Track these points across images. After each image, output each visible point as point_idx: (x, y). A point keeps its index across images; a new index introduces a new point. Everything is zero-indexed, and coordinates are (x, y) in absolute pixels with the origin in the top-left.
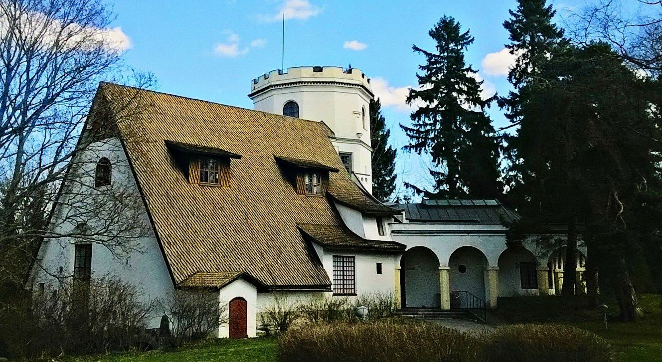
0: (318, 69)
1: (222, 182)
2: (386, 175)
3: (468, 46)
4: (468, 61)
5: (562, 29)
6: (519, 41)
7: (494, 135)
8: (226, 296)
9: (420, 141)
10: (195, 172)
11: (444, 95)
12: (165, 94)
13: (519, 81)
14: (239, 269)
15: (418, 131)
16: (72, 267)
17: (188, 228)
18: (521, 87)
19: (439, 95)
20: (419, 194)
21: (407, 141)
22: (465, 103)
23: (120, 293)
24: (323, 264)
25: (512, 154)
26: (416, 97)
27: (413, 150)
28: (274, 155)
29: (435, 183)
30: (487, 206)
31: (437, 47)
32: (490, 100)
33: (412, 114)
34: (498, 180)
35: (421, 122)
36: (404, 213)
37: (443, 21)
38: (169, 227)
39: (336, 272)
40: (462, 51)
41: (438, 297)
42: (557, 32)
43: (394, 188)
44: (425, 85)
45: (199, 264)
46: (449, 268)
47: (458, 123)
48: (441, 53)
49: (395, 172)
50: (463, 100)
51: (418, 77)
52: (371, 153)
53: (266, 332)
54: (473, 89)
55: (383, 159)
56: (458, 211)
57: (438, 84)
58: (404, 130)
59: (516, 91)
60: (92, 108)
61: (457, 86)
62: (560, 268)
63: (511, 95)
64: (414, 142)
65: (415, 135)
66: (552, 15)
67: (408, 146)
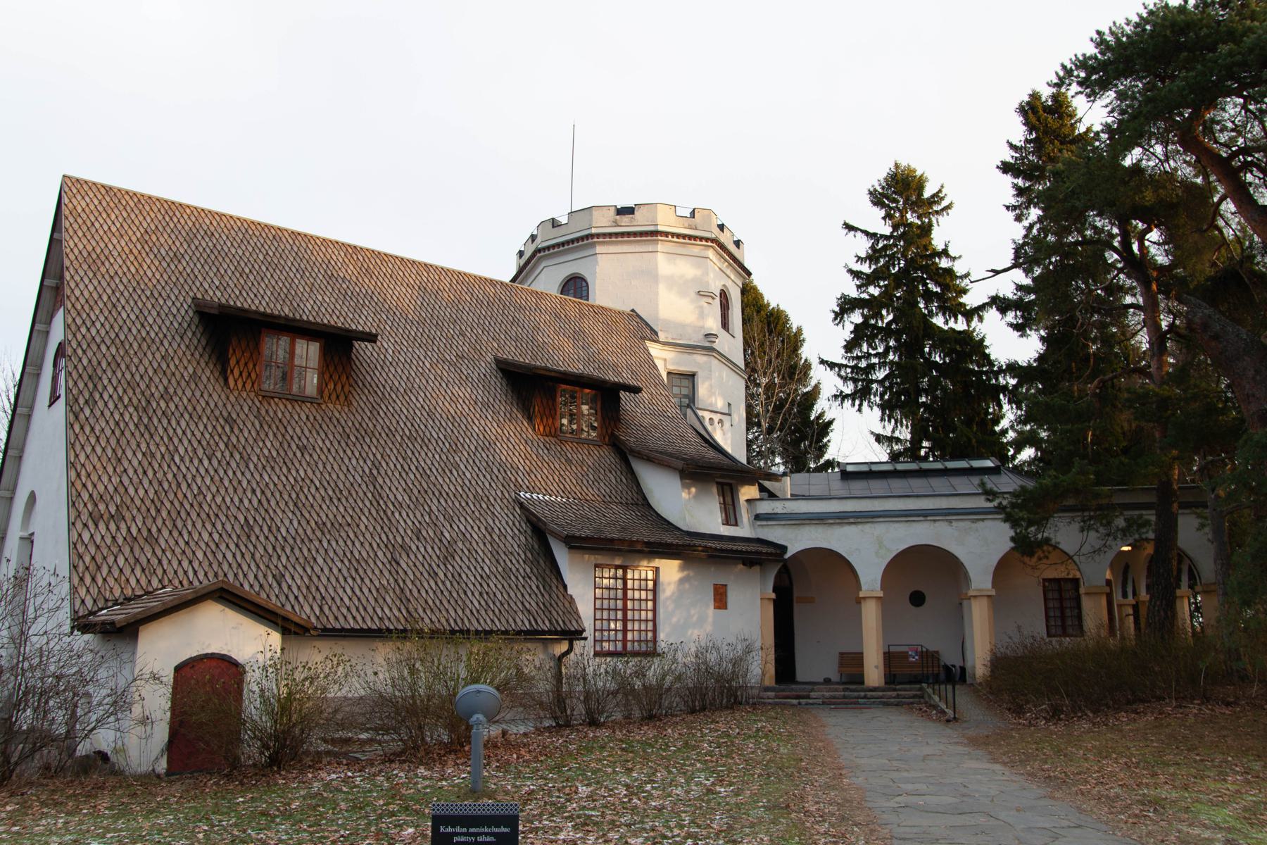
3: (940, 218)
15: (854, 368)
27: (847, 403)
31: (884, 218)
32: (982, 307)
62: (1125, 595)
64: (849, 389)
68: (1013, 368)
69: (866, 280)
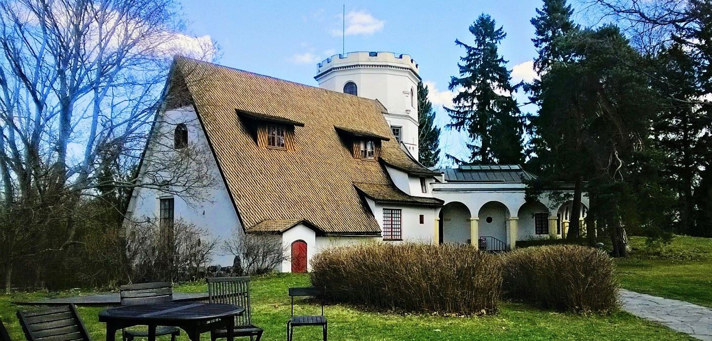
1: (287, 146)
2: (431, 149)
3: (501, 41)
4: (500, 53)
7: (519, 115)
8: (288, 239)
9: (460, 121)
10: (263, 137)
13: (541, 69)
15: (458, 112)
19: (476, 82)
20: (457, 164)
21: (449, 120)
25: (533, 130)
26: (457, 83)
27: (453, 128)
29: (470, 155)
31: (475, 41)
32: (518, 86)
35: (461, 105)
36: (443, 175)
37: (482, 19)
39: (386, 218)
41: (469, 241)
43: (438, 160)
45: (266, 214)
46: (478, 219)
51: (460, 66)
54: (504, 78)
55: (429, 136)
59: (539, 78)
62: (566, 219)
64: (455, 121)
65: (455, 115)
66: (571, 13)
68: (529, 116)
69: (463, 70)
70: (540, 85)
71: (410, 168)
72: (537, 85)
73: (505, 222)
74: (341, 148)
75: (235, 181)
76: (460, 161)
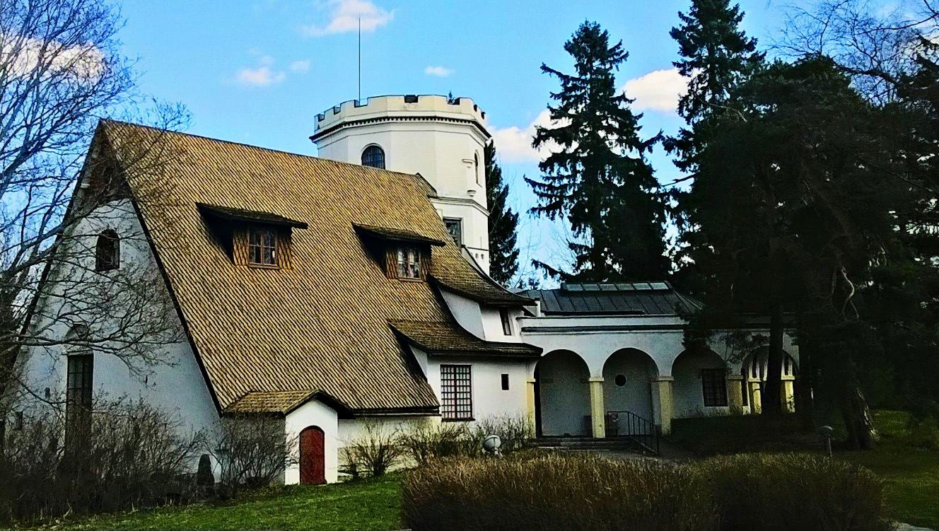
0: (411, 99)
2: (503, 250)
5: (753, 38)
6: (692, 56)
8: (295, 425)
9: (554, 201)
10: (241, 250)
11: (587, 134)
12: (195, 136)
13: (693, 113)
14: (310, 386)
15: (550, 187)
16: (63, 386)
17: (234, 329)
18: (695, 122)
21: (534, 201)
22: (616, 145)
23: (146, 424)
24: (427, 376)
26: (545, 138)
27: (543, 214)
28: (352, 223)
29: (574, 260)
30: (653, 292)
31: (576, 66)
32: (653, 141)
33: (541, 163)
34: (664, 254)
35: (554, 174)
36: (538, 303)
38: (208, 328)
39: (446, 388)
40: (611, 72)
41: (588, 420)
42: (747, 43)
43: (516, 268)
44: (560, 121)
47: (607, 174)
48: (581, 74)
49: (516, 246)
50: (614, 141)
52: (487, 218)
53: (352, 478)
54: (627, 124)
55: (502, 227)
56: (614, 299)
57: (577, 119)
58: (530, 186)
59: (690, 128)
60: (89, 154)
61: (605, 121)
62: (754, 376)
63: (682, 134)
64: (545, 202)
65: (546, 192)
66: (740, 19)
67: (537, 209)
69: (557, 114)
70: (691, 139)
71: (482, 291)
72: (687, 139)
73: (650, 384)
74: (364, 260)
75: (201, 325)
76: (556, 272)
